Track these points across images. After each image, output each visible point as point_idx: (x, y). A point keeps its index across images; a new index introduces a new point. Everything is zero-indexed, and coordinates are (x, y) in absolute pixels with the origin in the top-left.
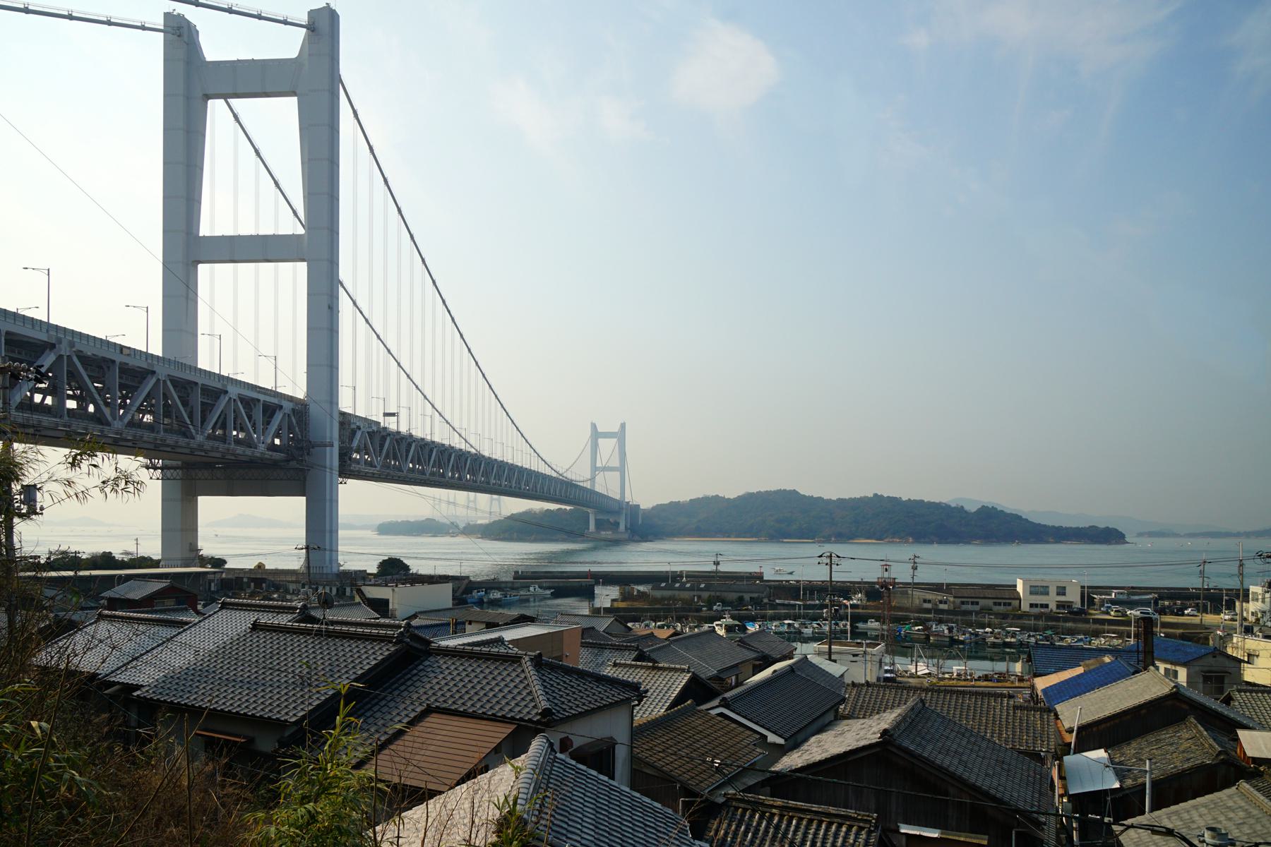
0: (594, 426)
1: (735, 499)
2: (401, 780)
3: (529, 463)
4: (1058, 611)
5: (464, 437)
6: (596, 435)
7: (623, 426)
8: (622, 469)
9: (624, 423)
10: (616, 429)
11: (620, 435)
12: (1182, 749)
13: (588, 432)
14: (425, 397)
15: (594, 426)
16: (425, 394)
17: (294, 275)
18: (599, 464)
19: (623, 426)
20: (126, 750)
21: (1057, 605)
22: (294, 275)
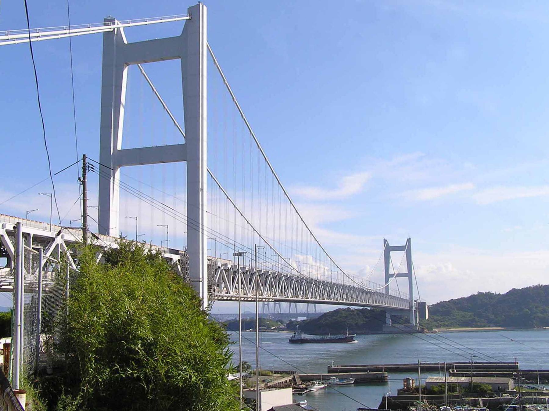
0: (385, 241)
6: (388, 249)
7: (409, 240)
8: (409, 275)
11: (407, 248)
15: (385, 241)
19: (409, 240)
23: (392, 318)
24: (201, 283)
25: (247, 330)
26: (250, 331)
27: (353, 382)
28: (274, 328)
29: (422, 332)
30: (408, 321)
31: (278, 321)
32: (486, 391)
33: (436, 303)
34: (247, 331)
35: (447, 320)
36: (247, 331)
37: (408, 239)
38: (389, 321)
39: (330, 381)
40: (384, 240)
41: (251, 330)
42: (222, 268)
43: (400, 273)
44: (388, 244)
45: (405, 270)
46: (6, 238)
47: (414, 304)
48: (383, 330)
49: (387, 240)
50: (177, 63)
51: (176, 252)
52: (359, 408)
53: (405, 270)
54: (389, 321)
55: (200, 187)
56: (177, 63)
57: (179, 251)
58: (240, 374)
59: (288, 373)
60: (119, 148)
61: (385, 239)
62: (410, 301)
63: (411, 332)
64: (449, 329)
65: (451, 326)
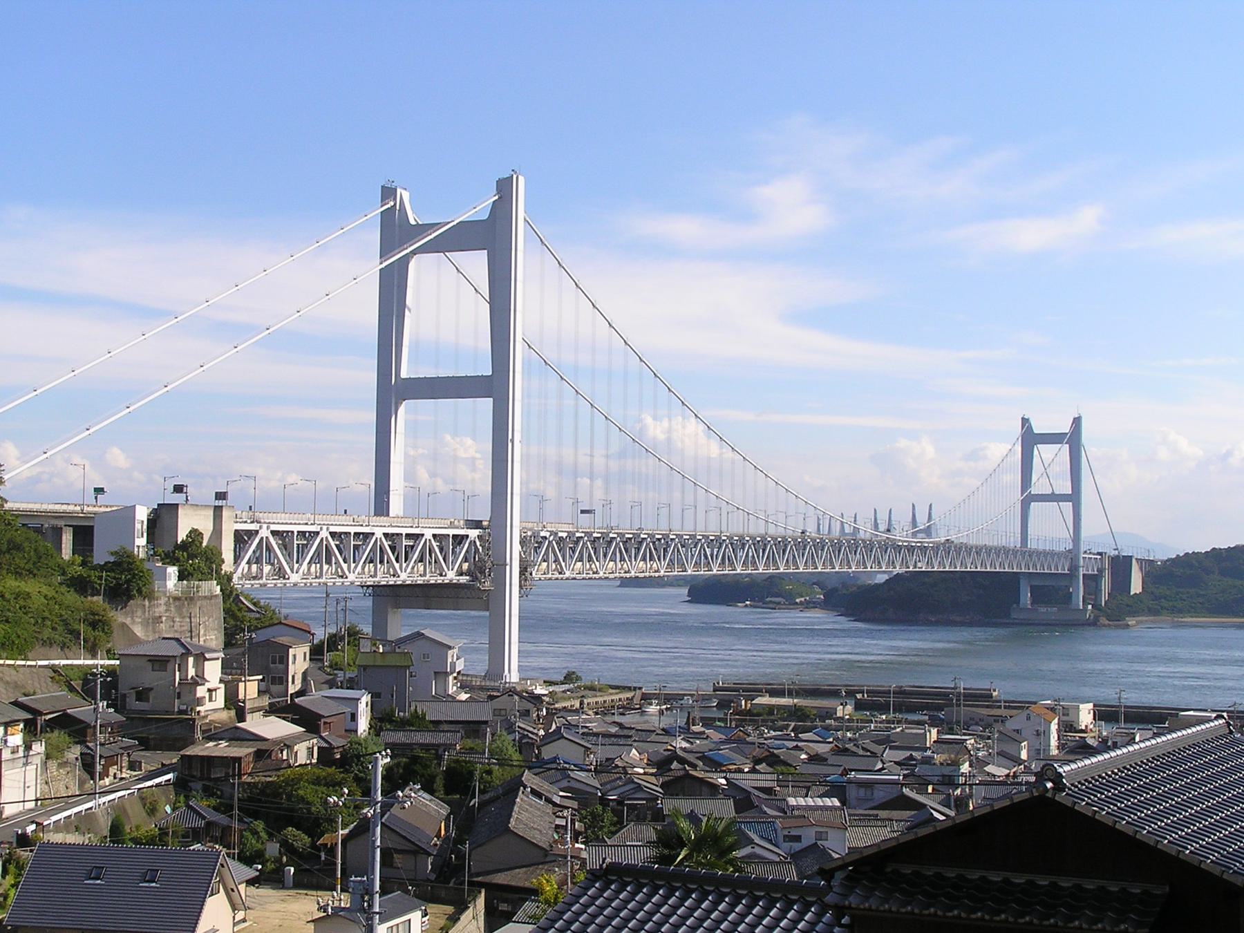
0: (1025, 421)
6: (1030, 439)
7: (1077, 422)
8: (1074, 497)
10: (1065, 428)
11: (1073, 439)
13: (1017, 430)
15: (1025, 421)
19: (1077, 422)
23: (1033, 589)
24: (508, 568)
25: (739, 604)
26: (746, 606)
27: (715, 704)
28: (803, 599)
29: (1094, 623)
30: (1068, 597)
31: (814, 584)
32: (809, 716)
33: (1174, 557)
34: (737, 606)
35: (1184, 597)
36: (737, 606)
37: (1074, 419)
38: (1026, 597)
39: (682, 702)
40: (1023, 418)
41: (748, 603)
42: (551, 538)
43: (1057, 492)
44: (1030, 428)
45: (1065, 488)
46: (271, 539)
47: (1082, 560)
48: (1012, 617)
49: (1028, 420)
50: (482, 257)
51: (477, 524)
52: (614, 722)
53: (1065, 488)
54: (1026, 597)
55: (510, 437)
56: (482, 257)
57: (481, 521)
58: (345, 673)
59: (629, 689)
60: (404, 375)
61: (1026, 417)
62: (1072, 556)
63: (1074, 624)
64: (1180, 619)
65: (1189, 612)
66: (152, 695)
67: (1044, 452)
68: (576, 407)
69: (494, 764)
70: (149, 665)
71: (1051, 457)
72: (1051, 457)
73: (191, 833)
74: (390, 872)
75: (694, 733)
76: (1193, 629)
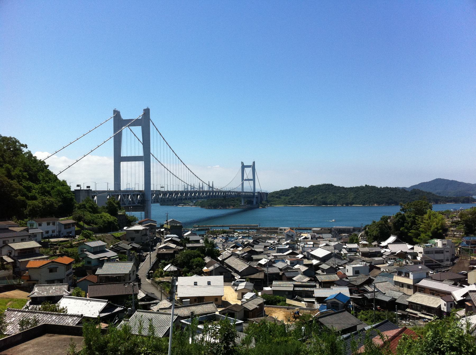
0: (242, 163)
1: (473, 184)
2: (374, 294)
3: (190, 182)
4: (312, 289)
5: (175, 175)
6: (243, 167)
7: (254, 163)
8: (254, 180)
9: (254, 162)
10: (251, 164)
11: (253, 167)
12: (31, 231)
13: (240, 166)
14: (165, 167)
15: (242, 163)
16: (165, 166)
17: (124, 153)
18: (245, 178)
19: (254, 163)
20: (300, 242)
21: (30, 225)
22: (124, 153)
62: (254, 193)
66: (135, 239)
67: (246, 169)
68: (167, 173)
69: (17, 325)
70: (134, 232)
71: (248, 172)
72: (248, 172)
73: (197, 299)
74: (415, 318)
75: (67, 254)
76: (14, 248)
